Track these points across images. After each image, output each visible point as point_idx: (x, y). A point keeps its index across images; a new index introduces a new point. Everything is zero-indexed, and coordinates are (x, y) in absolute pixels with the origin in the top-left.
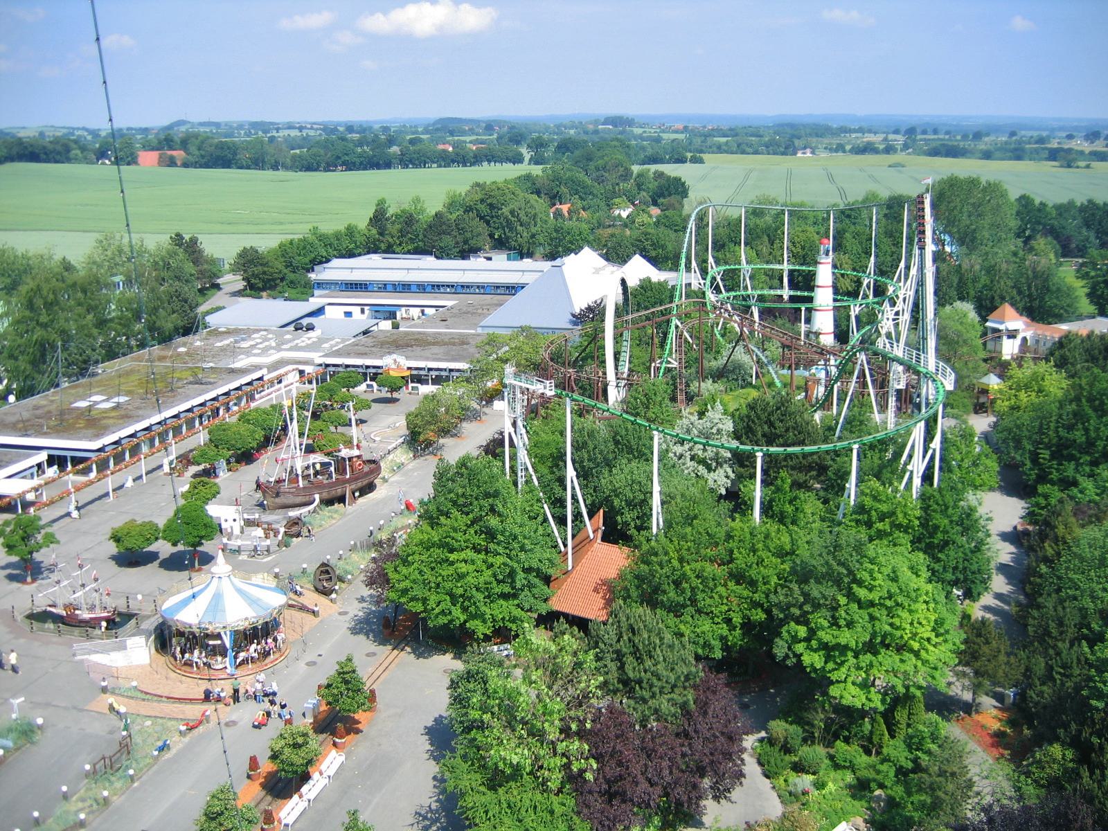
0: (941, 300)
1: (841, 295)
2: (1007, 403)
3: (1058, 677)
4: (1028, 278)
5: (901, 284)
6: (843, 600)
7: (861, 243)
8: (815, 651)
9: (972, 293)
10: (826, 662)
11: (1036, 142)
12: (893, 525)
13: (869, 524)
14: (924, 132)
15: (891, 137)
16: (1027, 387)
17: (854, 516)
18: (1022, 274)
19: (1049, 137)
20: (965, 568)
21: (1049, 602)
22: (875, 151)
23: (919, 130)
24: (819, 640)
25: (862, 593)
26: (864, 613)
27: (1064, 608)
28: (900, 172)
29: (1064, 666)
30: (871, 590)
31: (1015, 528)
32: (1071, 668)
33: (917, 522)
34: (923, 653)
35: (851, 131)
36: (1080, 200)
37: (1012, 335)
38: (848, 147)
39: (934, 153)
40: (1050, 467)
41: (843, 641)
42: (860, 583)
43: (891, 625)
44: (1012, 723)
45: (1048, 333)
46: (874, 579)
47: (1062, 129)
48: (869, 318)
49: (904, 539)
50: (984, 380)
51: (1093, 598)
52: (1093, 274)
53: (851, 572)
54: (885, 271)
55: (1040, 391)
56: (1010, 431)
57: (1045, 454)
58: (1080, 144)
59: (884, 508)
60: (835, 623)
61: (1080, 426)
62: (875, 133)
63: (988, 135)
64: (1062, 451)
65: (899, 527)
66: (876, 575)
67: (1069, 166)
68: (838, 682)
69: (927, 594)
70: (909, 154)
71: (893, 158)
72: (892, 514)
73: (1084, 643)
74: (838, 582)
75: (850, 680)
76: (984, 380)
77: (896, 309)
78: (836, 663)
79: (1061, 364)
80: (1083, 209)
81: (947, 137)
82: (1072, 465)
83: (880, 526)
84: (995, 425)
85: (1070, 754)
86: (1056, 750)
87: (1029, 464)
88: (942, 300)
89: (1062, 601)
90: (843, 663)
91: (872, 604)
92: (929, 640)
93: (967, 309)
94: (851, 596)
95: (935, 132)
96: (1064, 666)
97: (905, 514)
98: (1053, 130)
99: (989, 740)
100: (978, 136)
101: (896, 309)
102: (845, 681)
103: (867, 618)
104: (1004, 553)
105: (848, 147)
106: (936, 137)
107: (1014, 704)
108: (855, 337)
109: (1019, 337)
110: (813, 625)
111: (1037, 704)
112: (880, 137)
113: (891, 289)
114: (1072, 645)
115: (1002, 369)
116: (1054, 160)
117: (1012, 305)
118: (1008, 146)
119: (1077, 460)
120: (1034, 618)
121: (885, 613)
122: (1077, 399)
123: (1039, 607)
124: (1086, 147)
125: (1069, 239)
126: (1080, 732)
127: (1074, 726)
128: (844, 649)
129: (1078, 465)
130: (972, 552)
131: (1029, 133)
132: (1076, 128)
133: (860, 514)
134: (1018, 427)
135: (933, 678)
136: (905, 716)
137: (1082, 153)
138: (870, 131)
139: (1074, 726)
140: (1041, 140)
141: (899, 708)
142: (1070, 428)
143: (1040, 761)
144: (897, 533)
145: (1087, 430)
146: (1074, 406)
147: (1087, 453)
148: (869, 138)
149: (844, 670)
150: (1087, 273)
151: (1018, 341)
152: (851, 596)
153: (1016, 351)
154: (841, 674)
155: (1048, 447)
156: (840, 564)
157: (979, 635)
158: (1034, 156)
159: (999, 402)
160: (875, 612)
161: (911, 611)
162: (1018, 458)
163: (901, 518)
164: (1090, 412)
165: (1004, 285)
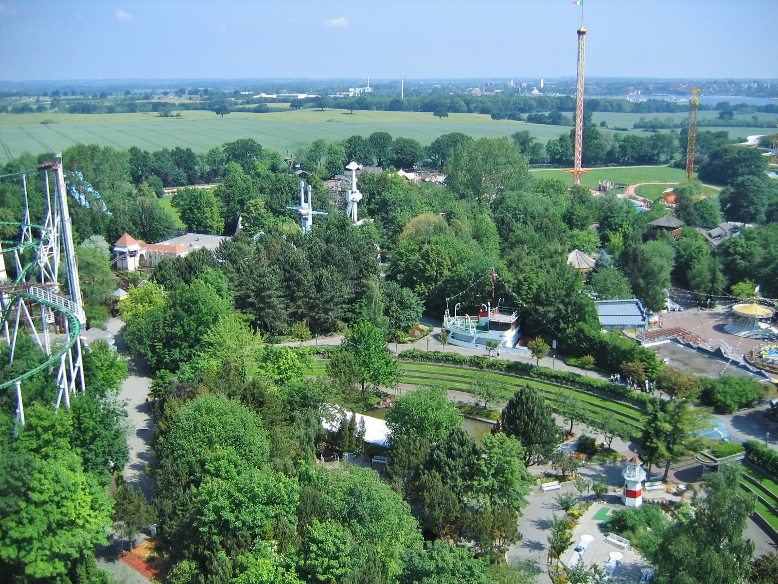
0: (78, 242)
1: (9, 239)
2: (130, 313)
3: (180, 513)
4: (139, 213)
5: (51, 228)
6: (23, 504)
7: (19, 199)
8: (9, 546)
9: (103, 227)
10: (19, 552)
11: (144, 99)
12: (54, 435)
13: (38, 436)
14: (66, 94)
15: (42, 98)
16: (142, 300)
17: (26, 433)
18: (135, 210)
19: (152, 93)
20: (110, 451)
21: (167, 462)
22: (31, 110)
23: (61, 92)
24: (11, 538)
25: (35, 496)
26: (40, 510)
27: (177, 465)
28: (49, 128)
29: (183, 505)
30: (41, 492)
31: (147, 400)
32: (186, 505)
33: (72, 428)
34: (87, 525)
35: (11, 95)
36: (171, 148)
37: (133, 254)
38: (10, 108)
39: (73, 110)
40: (164, 354)
41: (27, 535)
42: (33, 490)
43: (62, 513)
44: (157, 549)
45: (156, 251)
46: (43, 485)
47: (160, 87)
48: (31, 256)
49: (64, 442)
50: (116, 294)
51: (194, 454)
52: (182, 203)
53: (24, 484)
54: (39, 218)
55: (151, 302)
56: (134, 333)
57: (159, 345)
58: (172, 99)
59: (46, 423)
60: (20, 522)
61: (178, 324)
62: (30, 96)
63: (110, 94)
64: (170, 342)
65: (59, 435)
66: (44, 481)
67: (166, 116)
68: (30, 562)
69: (83, 483)
70: (55, 112)
71: (44, 116)
72: (53, 426)
73: (192, 486)
74: (17, 492)
75: (39, 559)
76: (116, 294)
77: (49, 246)
78: (26, 551)
79: (161, 281)
80: (173, 154)
81: (82, 97)
82: (178, 350)
83: (45, 436)
84: (124, 329)
85: (194, 565)
86: (185, 565)
87: (150, 353)
88: (81, 236)
89: (175, 459)
90: (31, 549)
91: (44, 503)
92: (89, 515)
93: (100, 242)
94: (28, 500)
95: (73, 93)
96: (183, 505)
97: (63, 425)
98: (155, 88)
99: (144, 566)
100: (103, 95)
101: (49, 246)
102: (36, 561)
103: (42, 513)
104: (140, 420)
105: (10, 108)
106: (74, 97)
107: (157, 534)
108: (22, 272)
109: (138, 255)
110: (4, 528)
111: (170, 533)
112: (32, 99)
113: (44, 233)
114: (185, 491)
115: (128, 282)
116: (156, 111)
117: (130, 233)
118: (125, 103)
119: (180, 346)
120: (160, 475)
121: (55, 506)
122: (173, 306)
123: (161, 467)
124: (177, 101)
125: (166, 175)
126: (197, 549)
127: (193, 547)
128: (30, 540)
129: (181, 349)
130: (113, 439)
131: (139, 91)
132: (169, 87)
133: (29, 430)
134: (139, 331)
135: (97, 539)
136: (84, 570)
137: (174, 105)
138: (25, 95)
139: (193, 547)
140: (147, 97)
141: (79, 565)
142: (172, 326)
143: (176, 575)
144: (58, 440)
145: (182, 326)
146: (173, 311)
147: (185, 341)
148: (25, 100)
149: (33, 553)
150: (178, 203)
151: (137, 258)
152: (28, 500)
153: (137, 264)
154: (32, 556)
155: (160, 340)
156: (17, 479)
157: (125, 498)
158: (143, 109)
159: (125, 313)
160: (48, 507)
161: (73, 500)
162: (142, 351)
163: (59, 429)
164: (183, 314)
165: (124, 220)
